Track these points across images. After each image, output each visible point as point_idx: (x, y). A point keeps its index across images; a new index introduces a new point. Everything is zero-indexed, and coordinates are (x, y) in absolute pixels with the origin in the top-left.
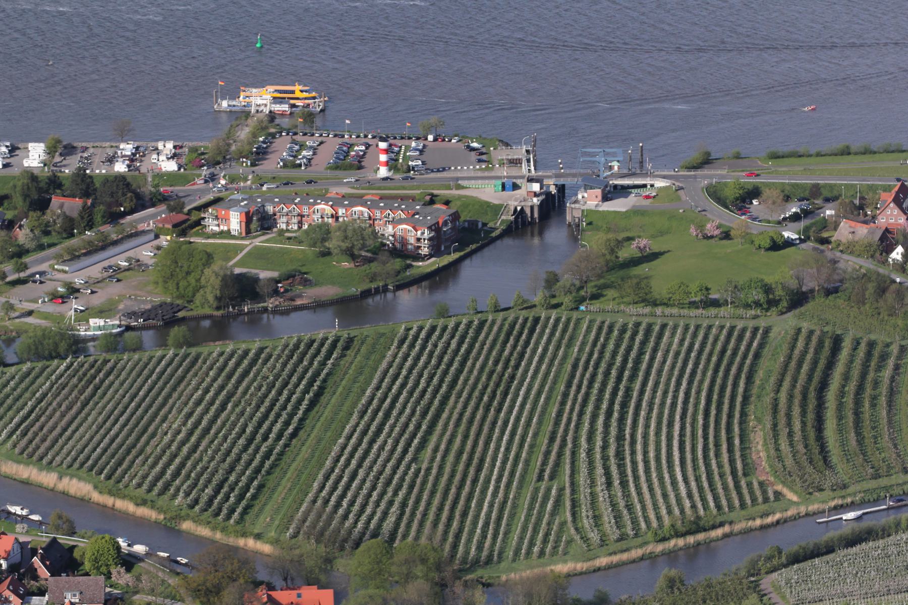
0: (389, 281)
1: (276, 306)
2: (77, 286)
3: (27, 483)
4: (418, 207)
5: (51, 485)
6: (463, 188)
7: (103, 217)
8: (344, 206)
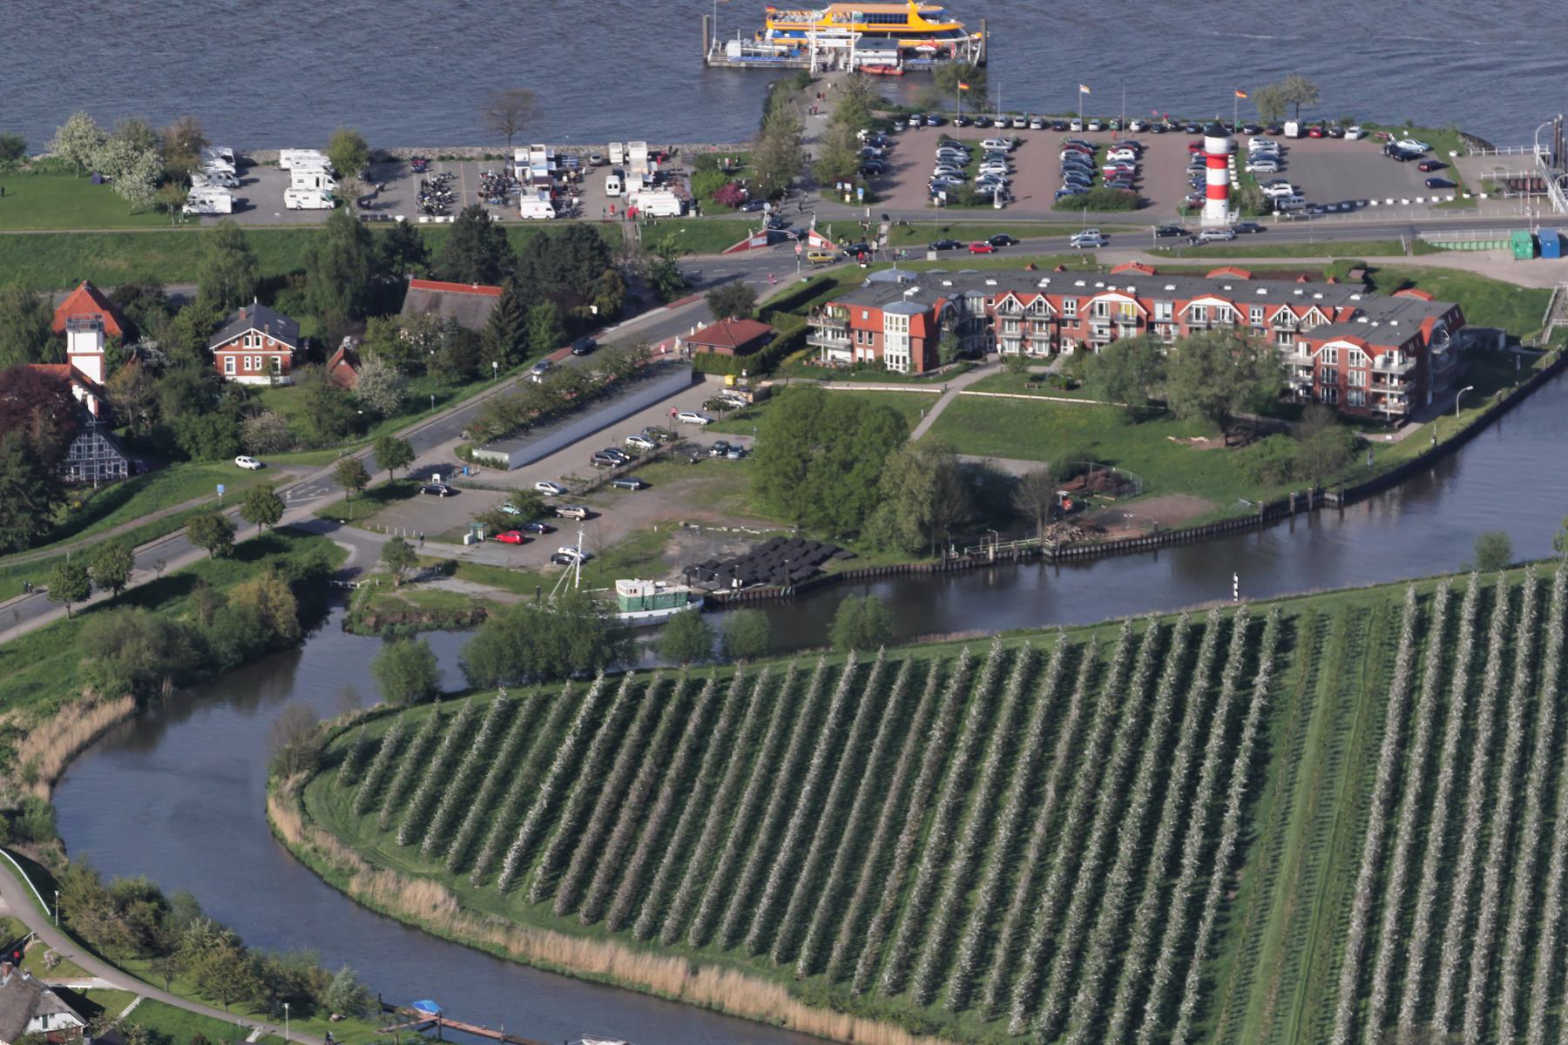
0: (1327, 481)
1: (1064, 546)
2: (549, 503)
3: (607, 985)
4: (1356, 297)
5: (674, 988)
6: (1433, 250)
7: (554, 329)
8: (1167, 297)
